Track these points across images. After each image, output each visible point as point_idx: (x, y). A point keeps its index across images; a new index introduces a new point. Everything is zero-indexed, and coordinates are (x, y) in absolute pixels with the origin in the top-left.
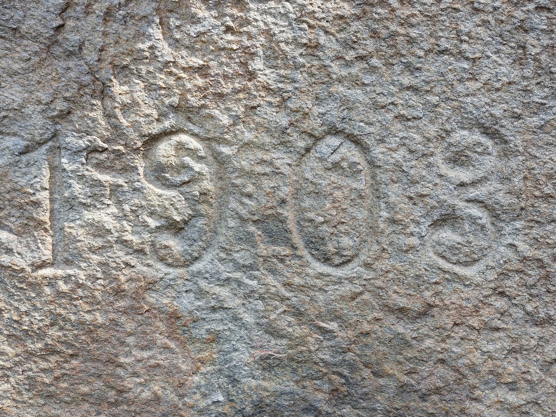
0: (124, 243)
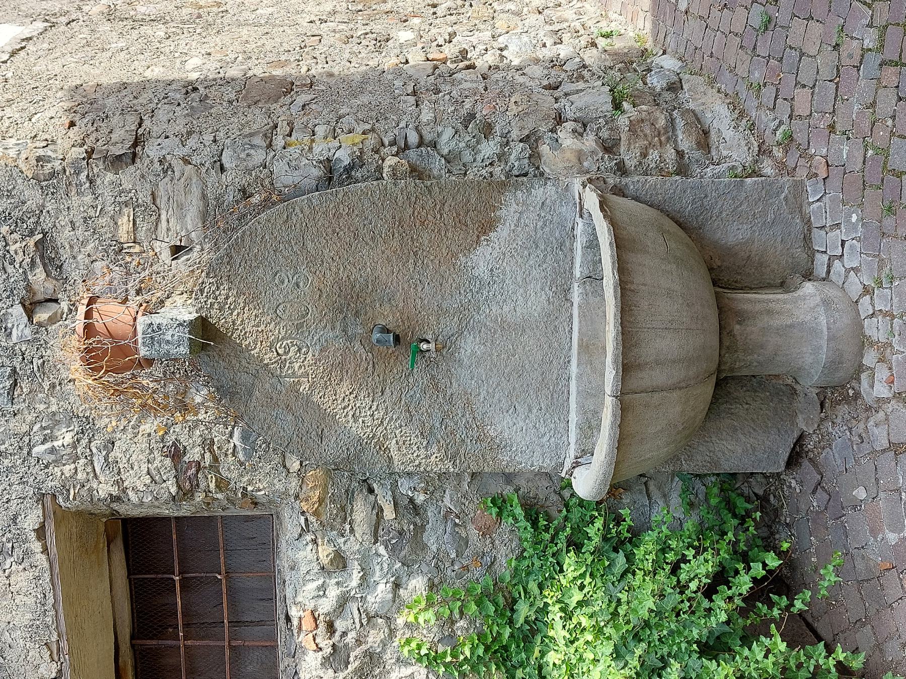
0: (303, 362)
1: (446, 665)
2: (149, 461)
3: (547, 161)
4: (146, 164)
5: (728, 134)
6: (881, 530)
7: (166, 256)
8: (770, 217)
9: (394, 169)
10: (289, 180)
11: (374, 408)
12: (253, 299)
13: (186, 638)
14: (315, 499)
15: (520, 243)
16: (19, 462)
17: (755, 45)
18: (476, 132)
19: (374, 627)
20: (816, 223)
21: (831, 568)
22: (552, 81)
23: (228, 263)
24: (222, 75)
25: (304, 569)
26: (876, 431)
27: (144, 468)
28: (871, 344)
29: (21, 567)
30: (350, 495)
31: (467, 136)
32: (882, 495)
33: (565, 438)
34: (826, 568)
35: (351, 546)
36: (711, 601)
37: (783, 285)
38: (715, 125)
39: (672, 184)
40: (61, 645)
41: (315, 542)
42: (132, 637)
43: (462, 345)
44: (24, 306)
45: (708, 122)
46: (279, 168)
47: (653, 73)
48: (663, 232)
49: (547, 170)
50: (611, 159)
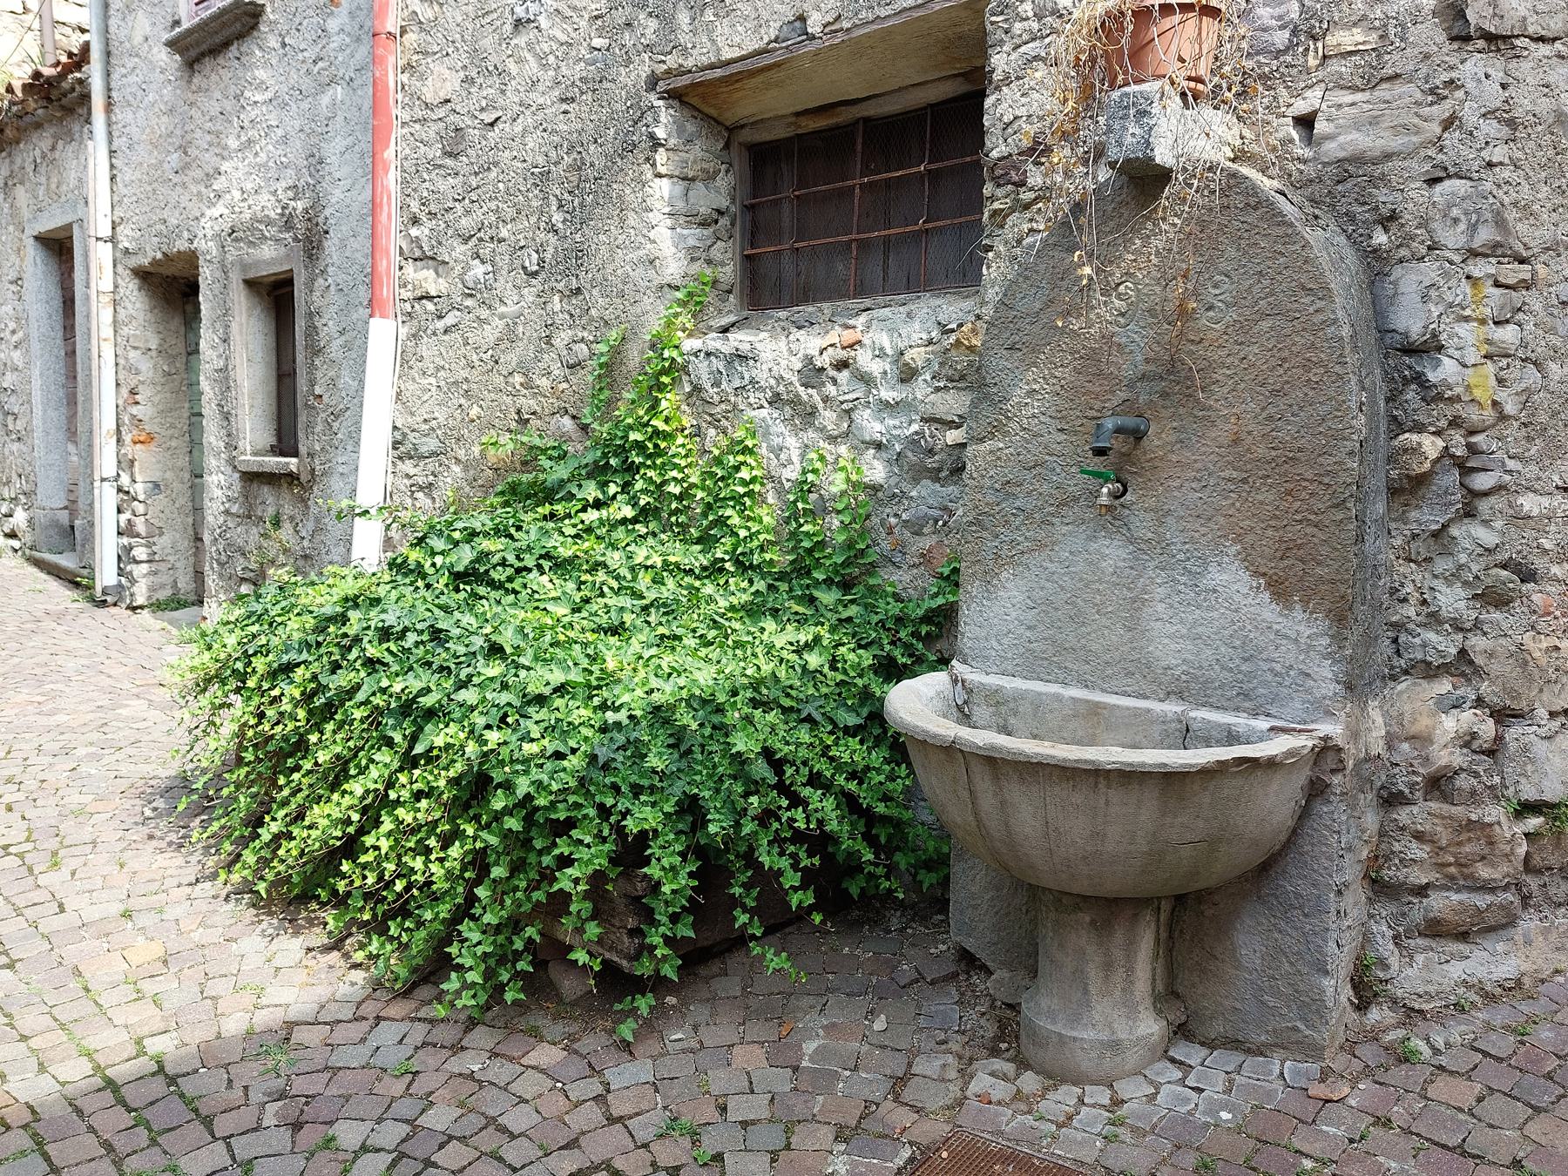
1: (795, 502)
3: (1418, 689)
4: (1447, 59)
5: (1456, 970)
7: (1301, 107)
8: (1271, 1001)
9: (1416, 450)
14: (974, 342)
15: (1252, 636)
19: (840, 417)
20: (1250, 1061)
23: (1248, 204)
27: (1022, 112)
31: (1478, 567)
32: (866, 1048)
33: (995, 669)
34: (788, 960)
35: (921, 389)
36: (753, 819)
37: (1169, 994)
38: (1477, 953)
39: (1326, 868)
40: (839, 34)
41: (930, 342)
42: (866, 120)
43: (1116, 543)
45: (1487, 944)
46: (1429, 271)
48: (1212, 843)
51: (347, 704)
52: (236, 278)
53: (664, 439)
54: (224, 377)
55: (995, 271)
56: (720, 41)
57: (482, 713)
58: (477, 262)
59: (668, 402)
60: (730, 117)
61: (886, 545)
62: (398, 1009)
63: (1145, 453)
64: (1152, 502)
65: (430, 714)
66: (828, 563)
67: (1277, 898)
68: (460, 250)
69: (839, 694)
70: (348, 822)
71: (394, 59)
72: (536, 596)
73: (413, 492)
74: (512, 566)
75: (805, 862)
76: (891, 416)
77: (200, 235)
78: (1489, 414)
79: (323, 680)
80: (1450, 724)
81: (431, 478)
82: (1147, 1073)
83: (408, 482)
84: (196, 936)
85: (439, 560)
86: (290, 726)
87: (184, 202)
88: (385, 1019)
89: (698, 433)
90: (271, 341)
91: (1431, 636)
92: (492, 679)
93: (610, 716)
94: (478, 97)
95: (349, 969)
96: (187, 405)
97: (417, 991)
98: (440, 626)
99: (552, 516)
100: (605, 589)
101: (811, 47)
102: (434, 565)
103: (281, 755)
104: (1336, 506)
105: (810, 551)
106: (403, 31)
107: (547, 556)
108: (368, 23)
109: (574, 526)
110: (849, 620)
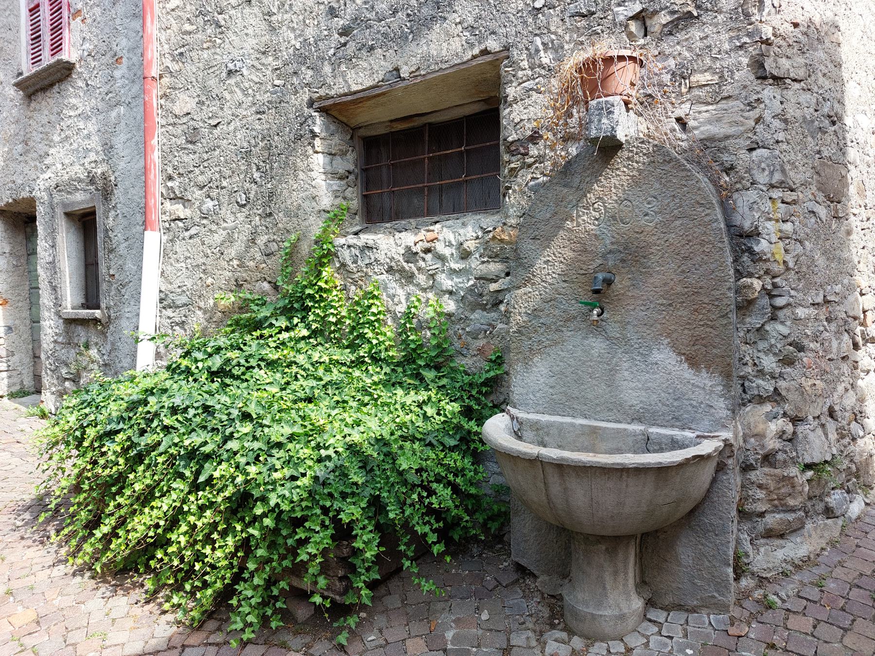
1: (405, 324)
2: (529, 119)
5: (780, 554)
6: (457, 626)
7: (680, 112)
9: (750, 287)
10: (740, 203)
11: (554, 275)
12: (635, 182)
13: (430, 158)
14: (503, 237)
16: (530, 28)
17: (861, 588)
18: (785, 353)
19: (428, 278)
20: (692, 617)
21: (433, 588)
22: (839, 414)
23: (665, 160)
24: (849, 144)
25: (462, 231)
26: (524, 637)
27: (525, 117)
28: (588, 646)
29: (464, 43)
30: (505, 260)
32: (480, 632)
33: (532, 410)
34: (434, 584)
35: (474, 263)
37: (642, 583)
41: (477, 238)
42: (430, 124)
44: (641, 12)
45: (792, 539)
47: (845, 495)
48: (678, 502)
49: (748, 409)
50: (756, 460)
51: (153, 454)
52: (59, 211)
53: (325, 292)
54: (53, 265)
55: (514, 201)
56: (350, 82)
57: (243, 455)
58: (209, 199)
59: (327, 272)
60: (354, 123)
61: (458, 345)
62: (196, 638)
63: (613, 292)
64: (618, 318)
65: (208, 457)
66: (425, 356)
67: (699, 526)
68: (198, 193)
69: (444, 428)
70: (157, 526)
71: (155, 92)
72: (258, 382)
73: (172, 327)
74: (243, 366)
75: (435, 526)
76: (457, 277)
77: (37, 188)
78: (782, 267)
79: (135, 439)
80: (774, 427)
81: (184, 318)
82: (639, 630)
83: (169, 321)
84: (56, 602)
85: (200, 365)
86: (115, 469)
87: (26, 170)
88: (188, 646)
89: (345, 288)
90: (81, 246)
91: (760, 382)
92: (246, 434)
93: (323, 453)
94: (206, 112)
95: (160, 614)
96: (28, 283)
97: (206, 625)
98: (208, 403)
99: (261, 336)
100: (299, 376)
101: (402, 84)
102: (197, 368)
103: (107, 485)
104: (723, 316)
105: (414, 350)
106: (161, 77)
107: (262, 359)
108: (139, 73)
109: (275, 342)
110: (444, 386)
